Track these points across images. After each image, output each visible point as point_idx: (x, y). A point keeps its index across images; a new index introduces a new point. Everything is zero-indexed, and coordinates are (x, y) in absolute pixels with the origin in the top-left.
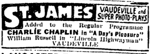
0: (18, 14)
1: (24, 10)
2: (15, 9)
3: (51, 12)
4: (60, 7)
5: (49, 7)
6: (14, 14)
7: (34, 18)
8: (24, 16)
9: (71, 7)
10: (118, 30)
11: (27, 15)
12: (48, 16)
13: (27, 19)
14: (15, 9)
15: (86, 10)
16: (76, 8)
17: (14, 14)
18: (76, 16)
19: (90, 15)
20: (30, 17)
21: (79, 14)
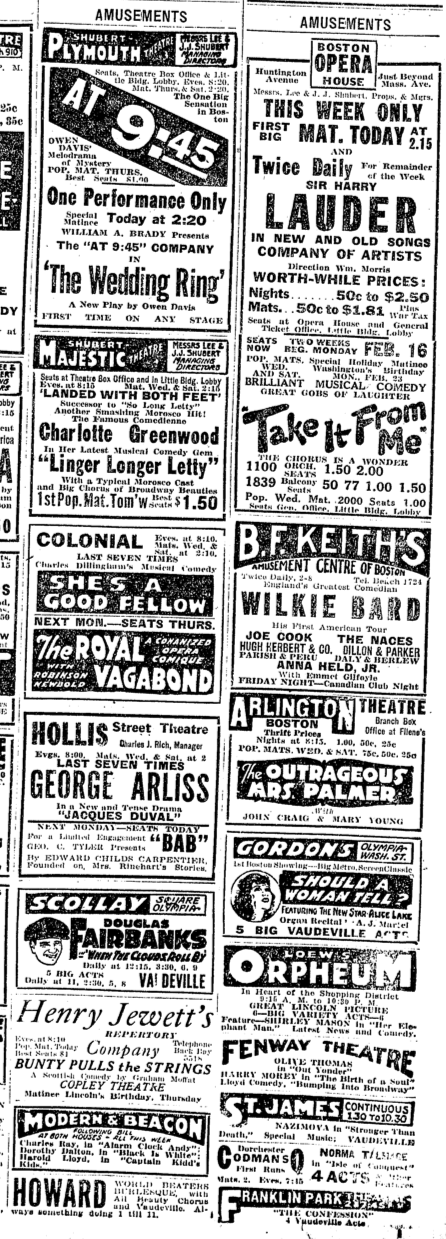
0: (242, 1107)
1: (251, 1102)
2: (238, 1100)
3: (180, 143)
4: (298, 1103)
5: (158, 137)
6: (237, 1105)
7: (264, 1115)
8: (250, 1110)
9: (312, 1103)
10: (373, 1136)
11: (255, 1109)
12: (282, 1112)
13: (255, 1115)
14: (238, 1100)
15: (333, 1105)
16: (319, 1103)
17: (237, 1105)
18: (337, 981)
19: (335, 1113)
20: (259, 1111)
21: (342, 978)
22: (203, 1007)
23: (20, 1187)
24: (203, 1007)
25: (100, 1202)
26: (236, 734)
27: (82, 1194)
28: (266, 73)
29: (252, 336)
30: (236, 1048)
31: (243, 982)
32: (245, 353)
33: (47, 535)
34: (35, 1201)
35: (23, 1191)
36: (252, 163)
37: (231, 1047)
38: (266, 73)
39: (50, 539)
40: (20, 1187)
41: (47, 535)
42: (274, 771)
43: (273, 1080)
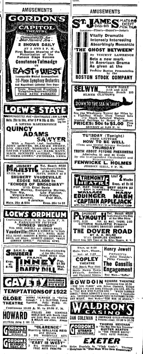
14: (43, 108)
22: (66, 340)
23: (5, 314)
24: (66, 340)
25: (26, 317)
26: (74, 29)
27: (21, 315)
28: (106, 71)
29: (63, 240)
30: (77, 162)
31: (9, 58)
32: (104, 246)
33: (79, 258)
34: (8, 317)
35: (5, 315)
36: (73, 231)
37: (65, 112)
38: (106, 71)
39: (79, 259)
40: (5, 314)
41: (79, 258)
42: (12, 214)
43: (125, 259)
